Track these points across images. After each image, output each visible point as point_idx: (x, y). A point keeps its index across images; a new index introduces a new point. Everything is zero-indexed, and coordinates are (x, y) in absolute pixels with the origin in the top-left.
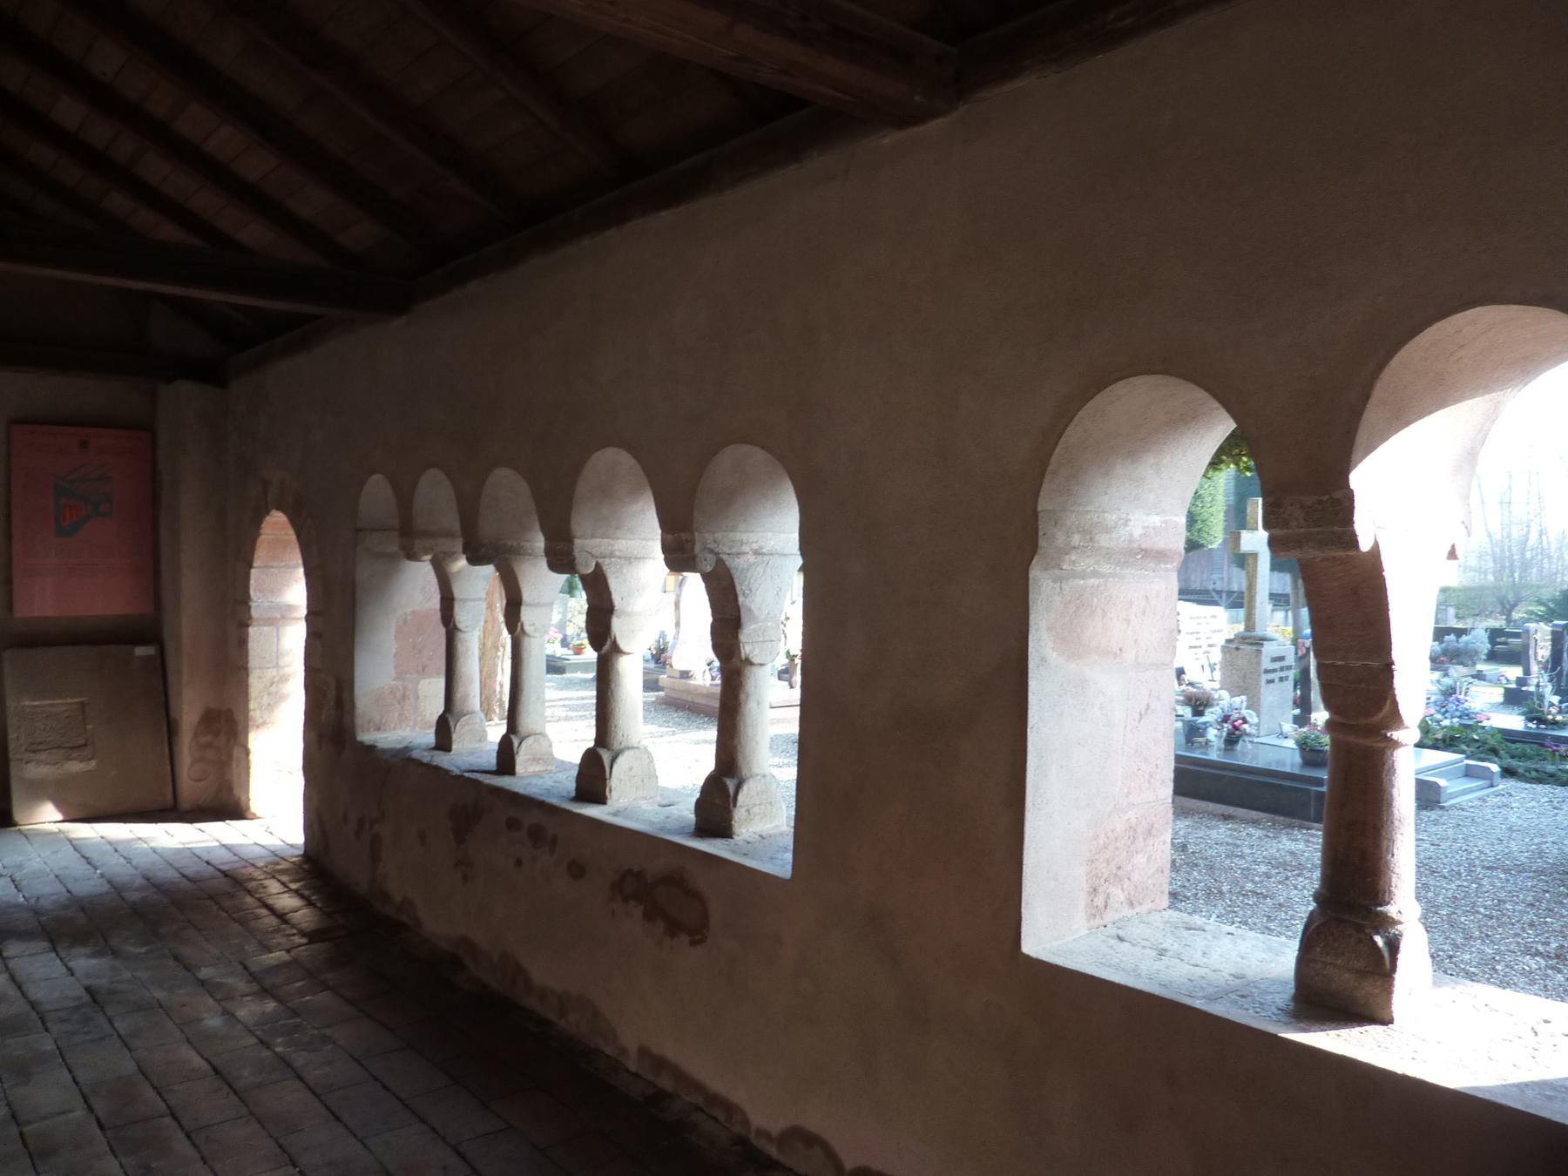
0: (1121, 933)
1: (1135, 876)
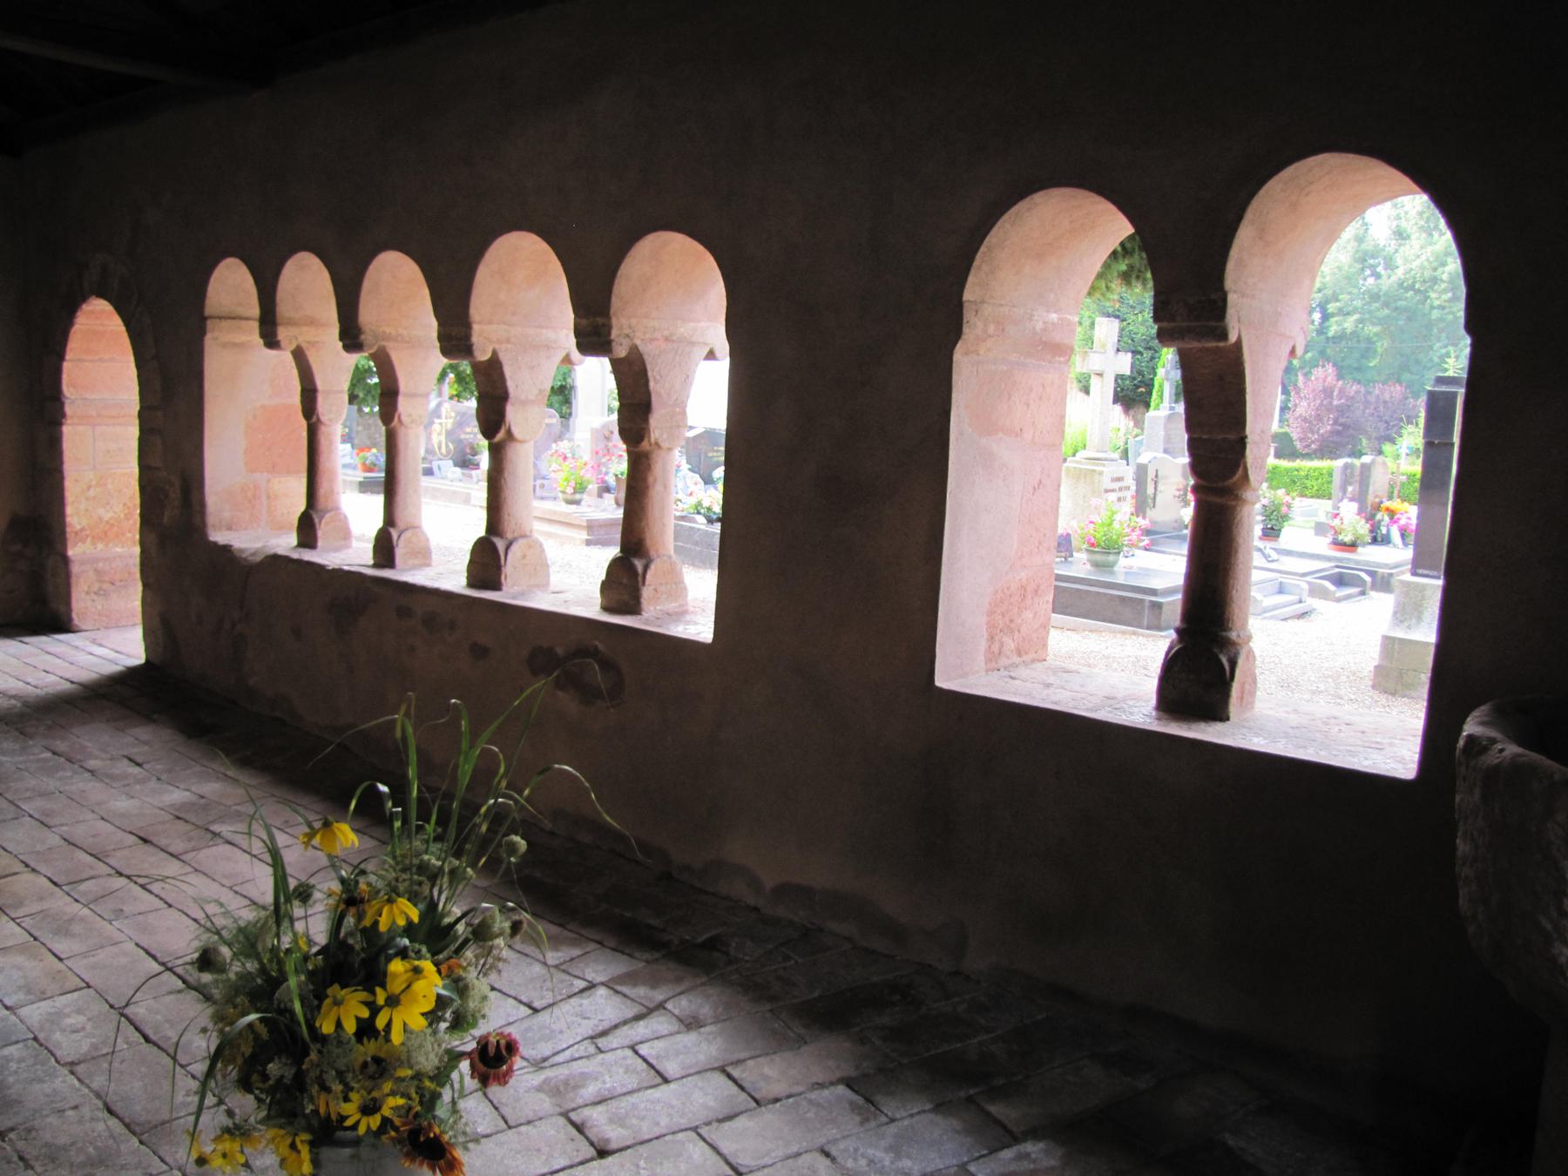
0: (1012, 674)
1: (1024, 629)
